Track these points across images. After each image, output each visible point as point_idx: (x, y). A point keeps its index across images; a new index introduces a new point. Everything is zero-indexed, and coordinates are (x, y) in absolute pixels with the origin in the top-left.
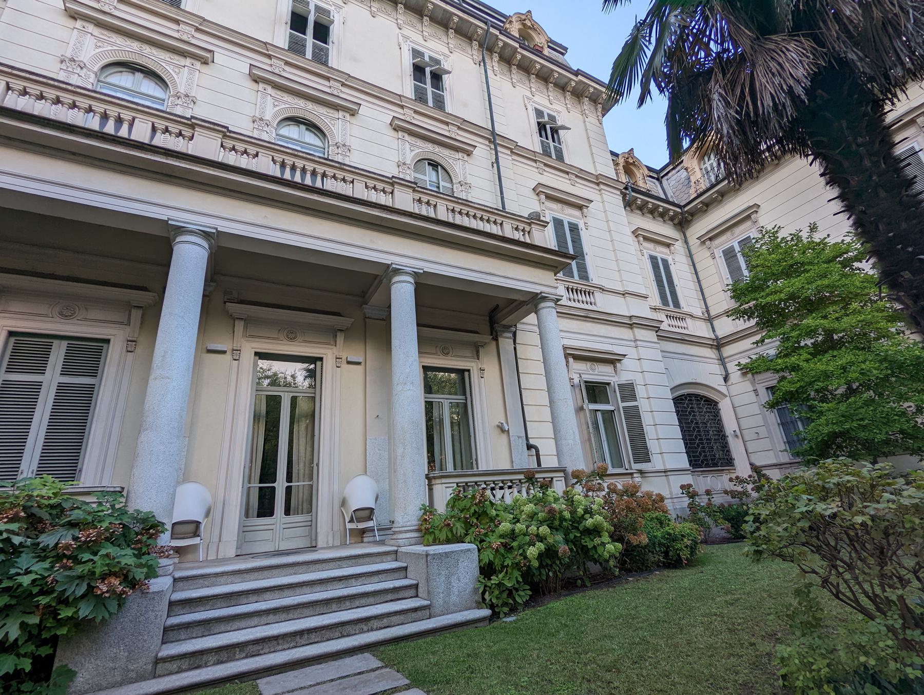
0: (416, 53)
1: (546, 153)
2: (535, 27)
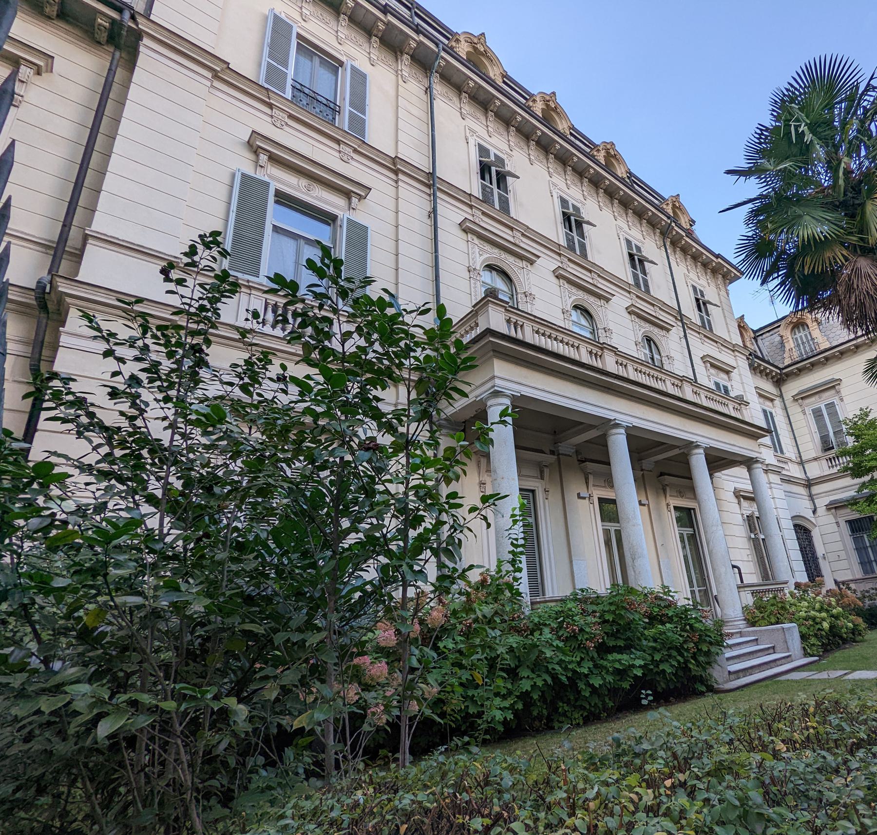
0: (483, 151)
1: (571, 247)
2: (486, 54)
